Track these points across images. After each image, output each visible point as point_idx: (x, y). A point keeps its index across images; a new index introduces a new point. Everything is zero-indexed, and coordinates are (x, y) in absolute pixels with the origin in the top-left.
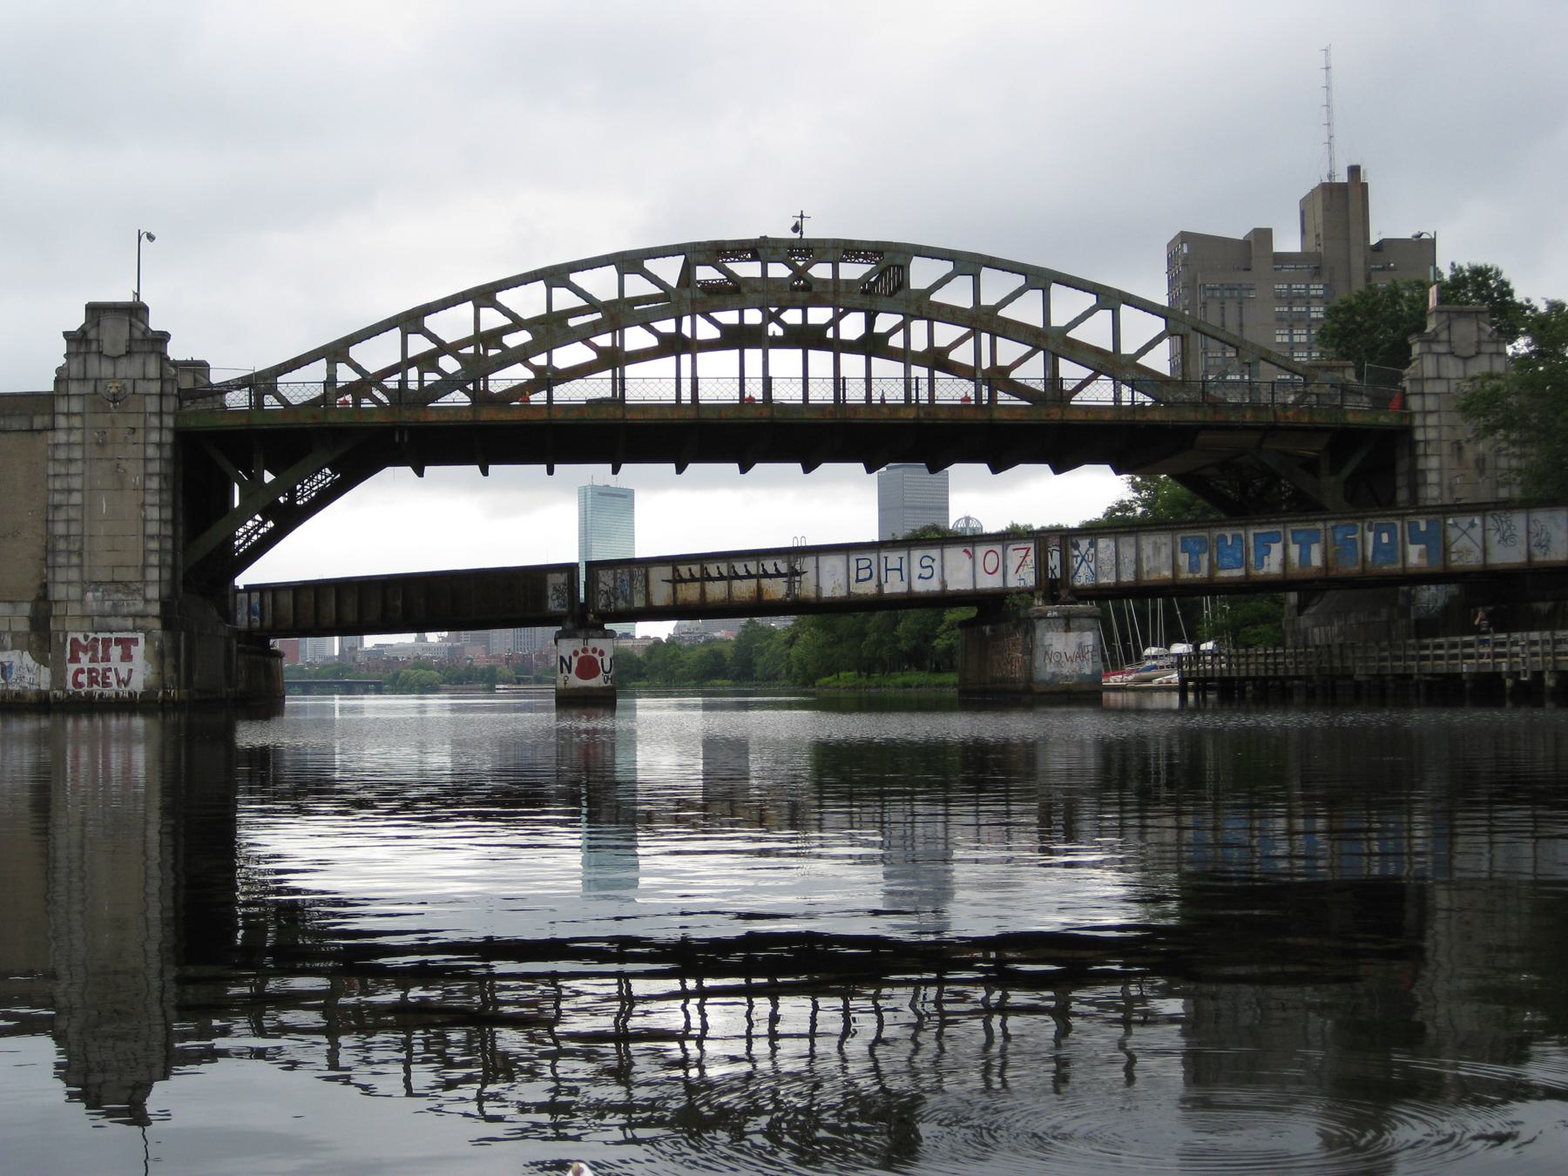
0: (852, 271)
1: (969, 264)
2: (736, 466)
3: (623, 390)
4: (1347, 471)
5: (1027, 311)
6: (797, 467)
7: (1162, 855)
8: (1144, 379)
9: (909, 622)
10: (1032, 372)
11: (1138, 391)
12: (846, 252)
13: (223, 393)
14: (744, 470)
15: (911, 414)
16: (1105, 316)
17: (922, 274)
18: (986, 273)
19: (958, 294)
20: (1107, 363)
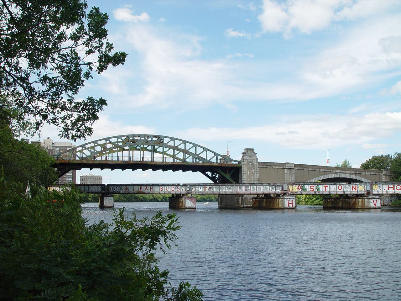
0: (155, 139)
1: (173, 139)
2: (90, 169)
3: (154, 159)
4: (231, 174)
5: (182, 147)
6: (89, 169)
7: (195, 273)
8: (200, 158)
9: (129, 201)
10: (203, 155)
11: (204, 159)
12: (154, 136)
13: (109, 139)
14: (91, 170)
15: (217, 165)
16: (194, 148)
17: (166, 141)
18: (176, 141)
19: (171, 144)
20: (194, 155)
